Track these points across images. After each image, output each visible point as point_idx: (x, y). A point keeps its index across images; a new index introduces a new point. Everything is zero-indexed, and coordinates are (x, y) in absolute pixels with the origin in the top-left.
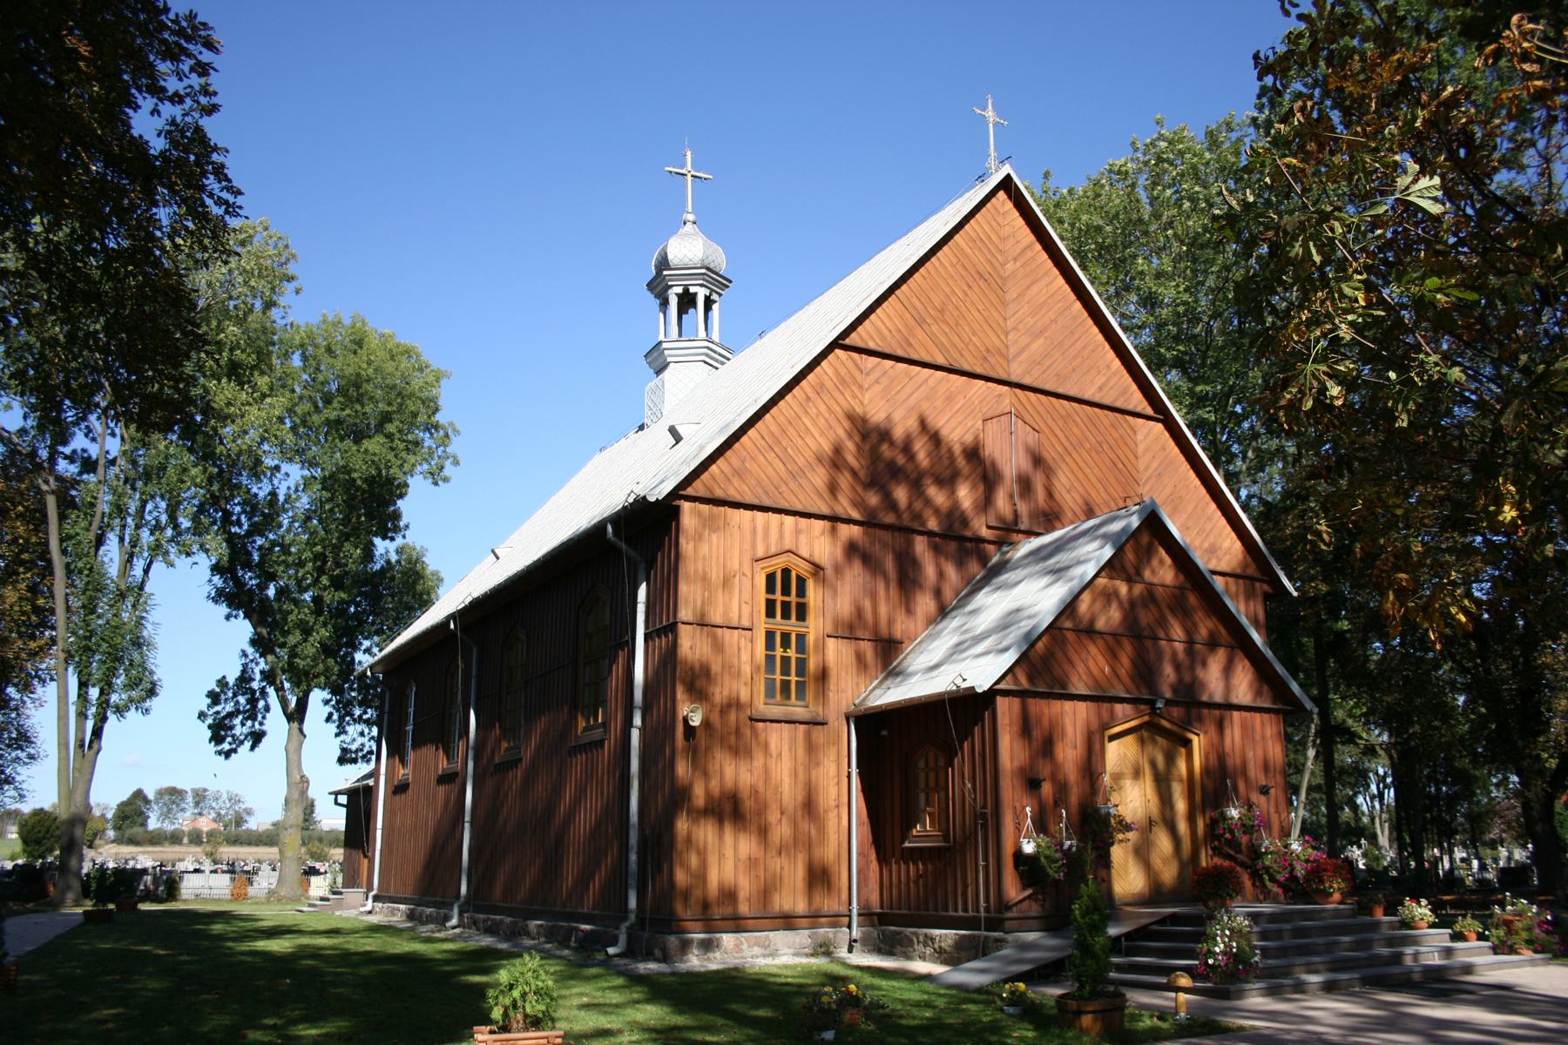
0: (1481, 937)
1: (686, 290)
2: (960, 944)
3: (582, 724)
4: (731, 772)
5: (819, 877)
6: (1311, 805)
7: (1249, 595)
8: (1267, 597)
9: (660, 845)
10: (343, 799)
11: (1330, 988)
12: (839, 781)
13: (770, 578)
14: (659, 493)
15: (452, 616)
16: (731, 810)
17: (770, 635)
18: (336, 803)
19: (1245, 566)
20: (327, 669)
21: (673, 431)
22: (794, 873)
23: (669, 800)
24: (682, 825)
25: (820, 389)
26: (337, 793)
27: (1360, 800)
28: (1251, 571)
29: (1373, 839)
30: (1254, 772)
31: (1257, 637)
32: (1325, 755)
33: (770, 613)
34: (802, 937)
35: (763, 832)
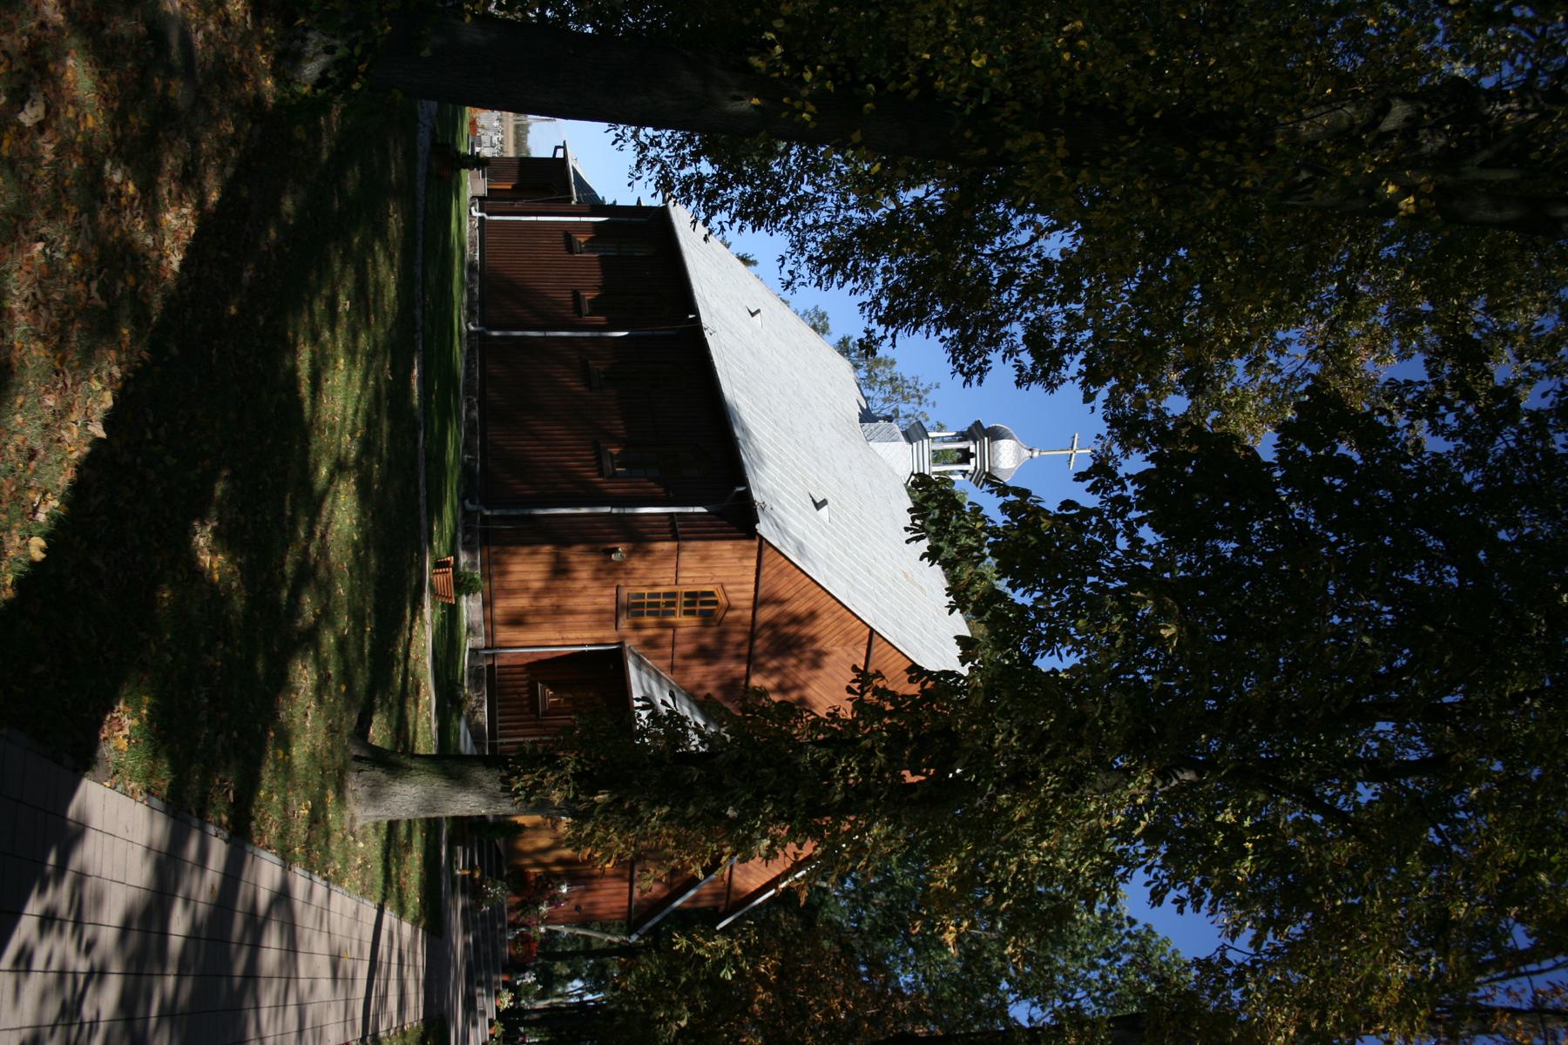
0: (492, 1036)
1: (973, 455)
2: (479, 726)
3: (615, 451)
4: (583, 573)
5: (517, 620)
6: (574, 938)
7: (717, 896)
8: (716, 908)
9: (534, 534)
10: (560, 154)
11: (466, 946)
12: (576, 636)
13: (711, 594)
14: (763, 528)
15: (698, 318)
16: (560, 570)
17: (674, 595)
18: (557, 148)
19: (738, 892)
20: (581, 802)
21: (824, 502)
22: (521, 602)
23: (561, 536)
24: (547, 548)
25: (841, 619)
26: (564, 147)
27: (578, 983)
28: (733, 897)
29: (541, 996)
30: (589, 898)
31: (678, 903)
32: (610, 950)
33: (687, 594)
34: (478, 617)
35: (546, 591)
